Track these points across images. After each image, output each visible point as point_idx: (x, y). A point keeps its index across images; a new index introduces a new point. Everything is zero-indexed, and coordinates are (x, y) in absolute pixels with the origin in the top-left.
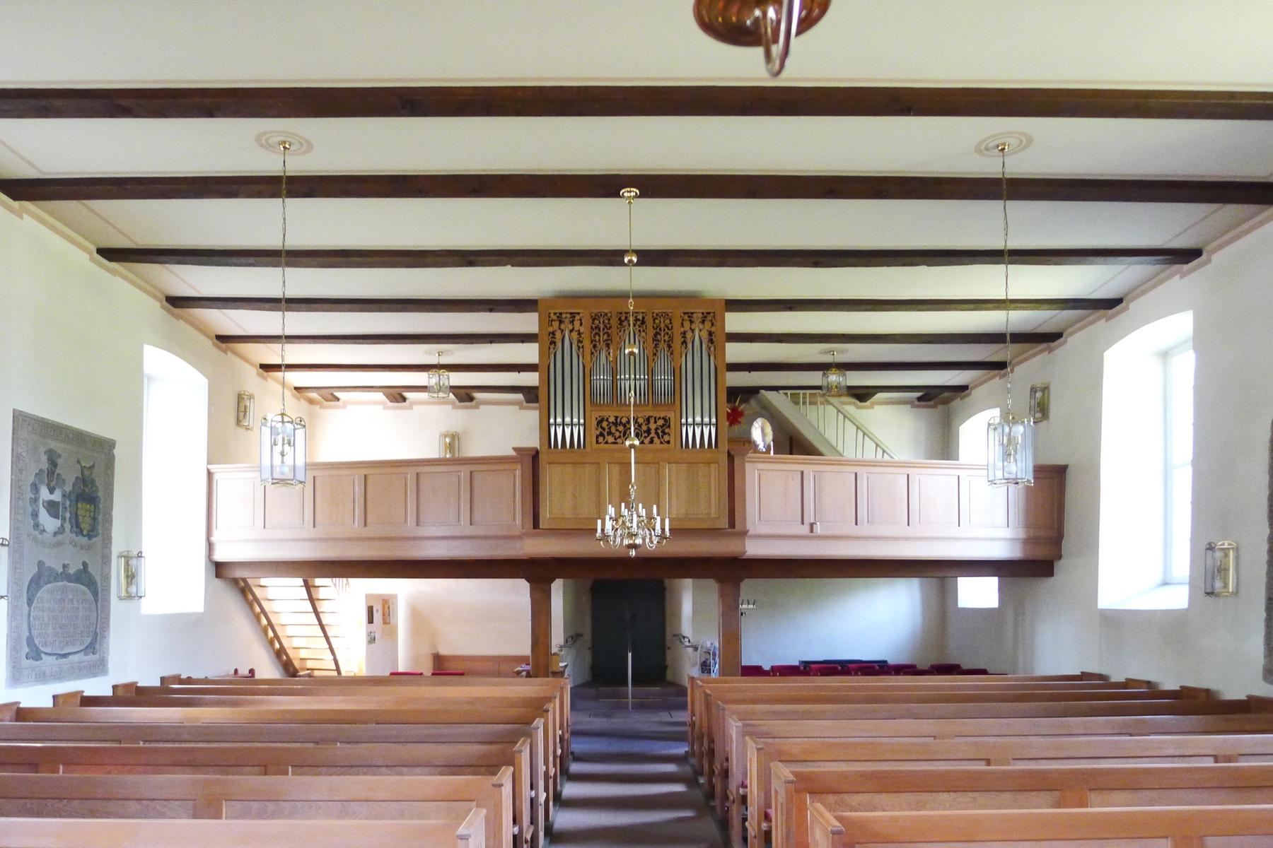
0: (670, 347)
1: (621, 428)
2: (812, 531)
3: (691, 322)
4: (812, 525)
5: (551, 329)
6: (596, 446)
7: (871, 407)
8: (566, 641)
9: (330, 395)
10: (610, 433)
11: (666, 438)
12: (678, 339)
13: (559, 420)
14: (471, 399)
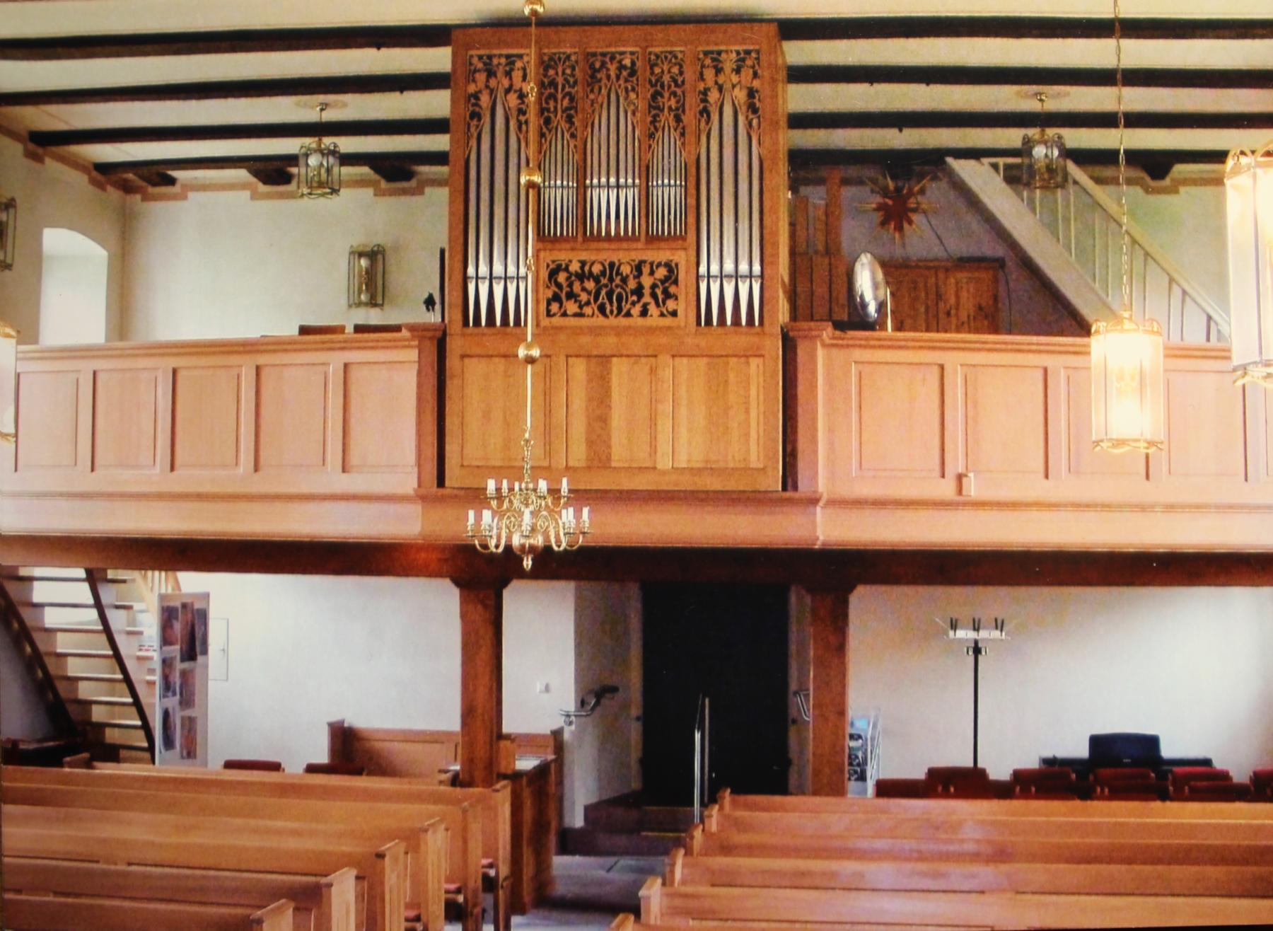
0: (678, 119)
1: (590, 285)
2: (960, 491)
3: (719, 71)
4: (960, 478)
5: (472, 88)
6: (545, 322)
7: (1173, 190)
8: (582, 703)
9: (158, 176)
10: (571, 296)
11: (671, 305)
12: (692, 102)
13: (484, 270)
14: (408, 176)
